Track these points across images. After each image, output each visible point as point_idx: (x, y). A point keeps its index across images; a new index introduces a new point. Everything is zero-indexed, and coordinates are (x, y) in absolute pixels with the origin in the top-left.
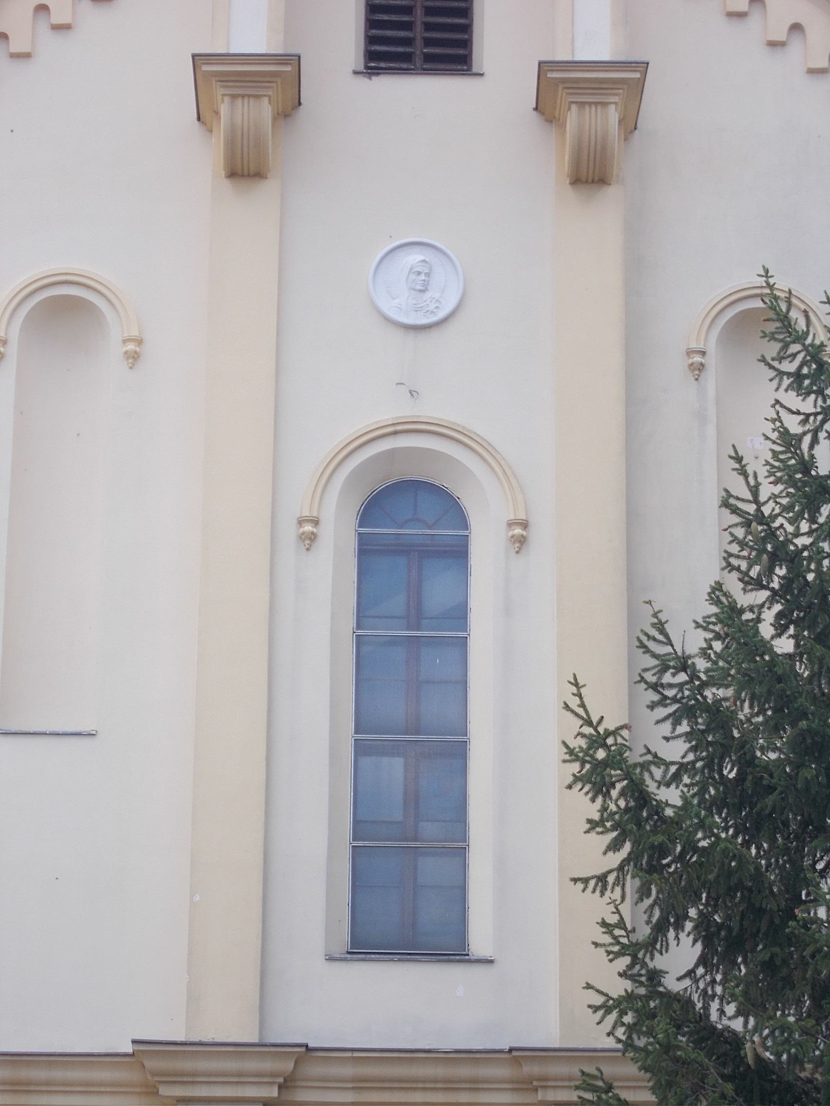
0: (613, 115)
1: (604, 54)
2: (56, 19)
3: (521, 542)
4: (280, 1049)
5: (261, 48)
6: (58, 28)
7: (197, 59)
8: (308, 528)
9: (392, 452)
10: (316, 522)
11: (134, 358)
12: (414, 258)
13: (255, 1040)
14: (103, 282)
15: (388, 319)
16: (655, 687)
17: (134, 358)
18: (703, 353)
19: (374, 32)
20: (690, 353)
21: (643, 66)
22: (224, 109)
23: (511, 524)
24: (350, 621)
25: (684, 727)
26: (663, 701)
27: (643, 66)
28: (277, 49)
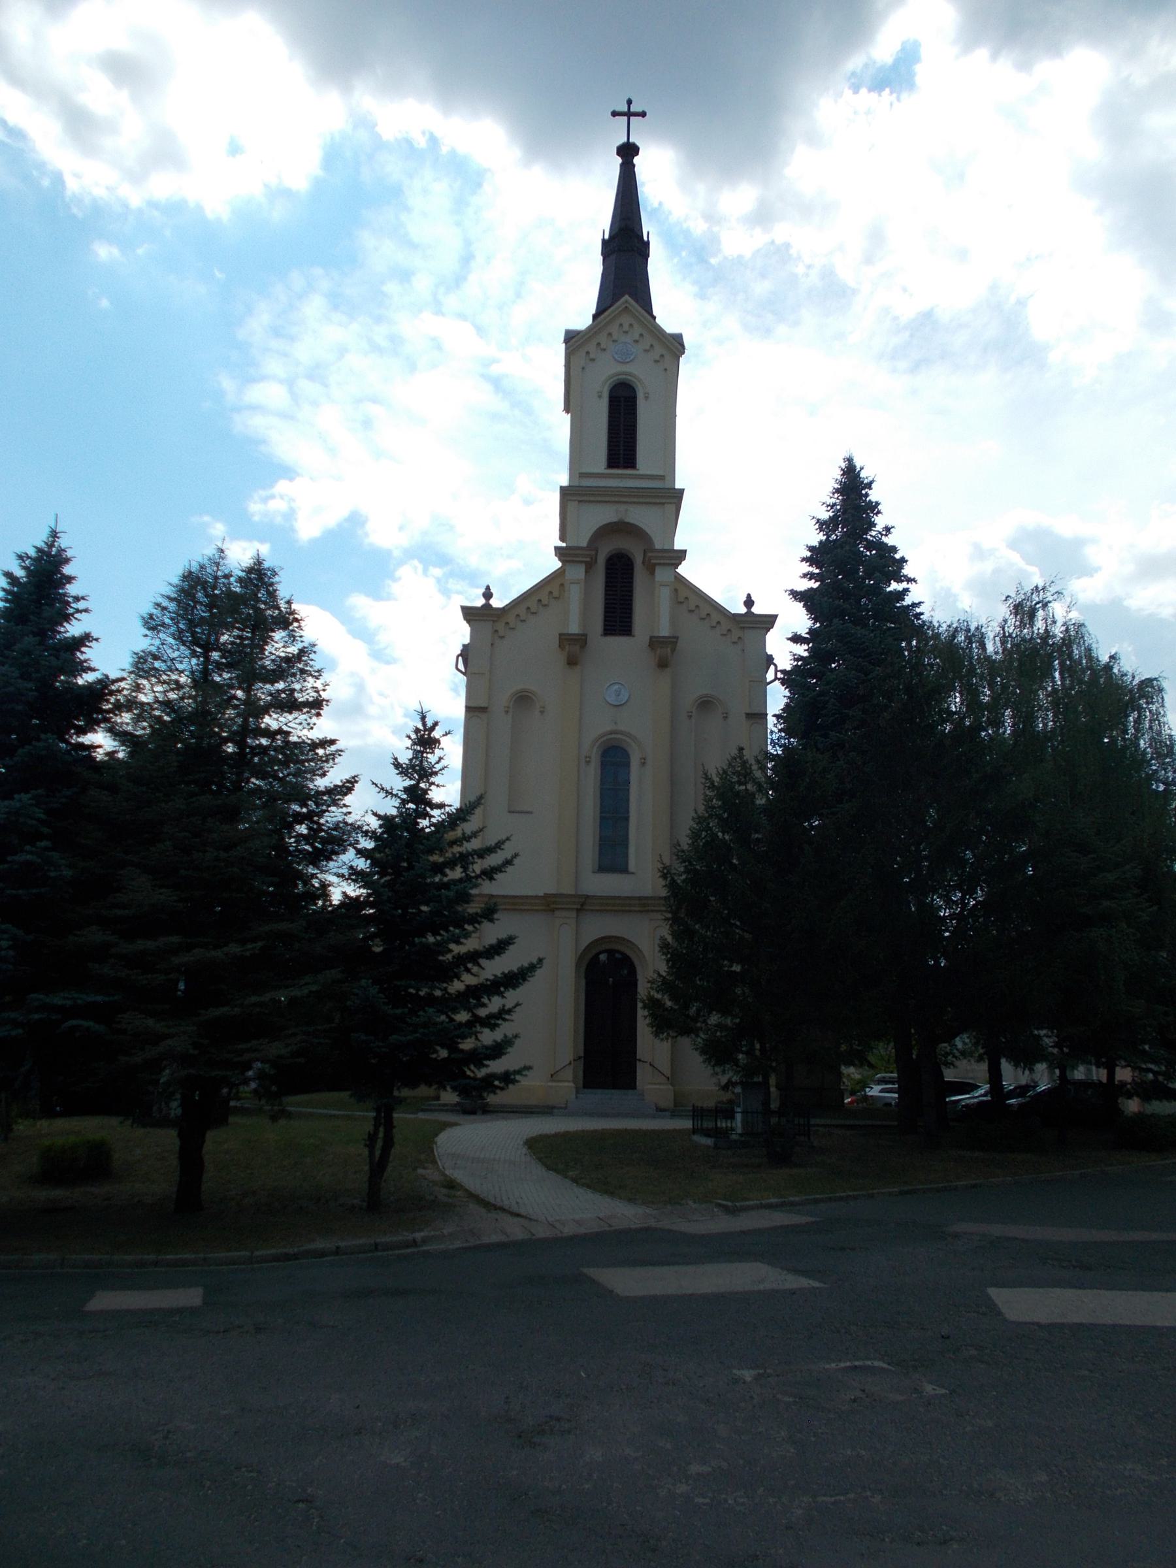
0: (669, 650)
1: (667, 635)
2: (522, 618)
3: (644, 764)
4: (580, 896)
5: (577, 632)
6: (522, 621)
7: (560, 635)
8: (588, 759)
9: (611, 739)
10: (590, 757)
11: (542, 712)
12: (616, 687)
13: (573, 893)
14: (571, 404)
15: (610, 704)
16: (677, 855)
17: (542, 712)
18: (692, 712)
19: (608, 597)
20: (688, 712)
21: (677, 638)
22: (567, 647)
23: (641, 759)
24: (598, 784)
25: (684, 864)
26: (678, 859)
27: (677, 638)
28: (581, 632)
